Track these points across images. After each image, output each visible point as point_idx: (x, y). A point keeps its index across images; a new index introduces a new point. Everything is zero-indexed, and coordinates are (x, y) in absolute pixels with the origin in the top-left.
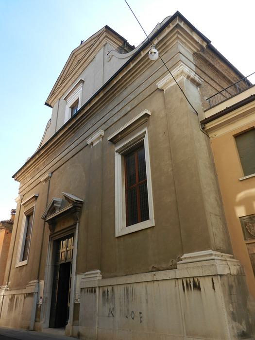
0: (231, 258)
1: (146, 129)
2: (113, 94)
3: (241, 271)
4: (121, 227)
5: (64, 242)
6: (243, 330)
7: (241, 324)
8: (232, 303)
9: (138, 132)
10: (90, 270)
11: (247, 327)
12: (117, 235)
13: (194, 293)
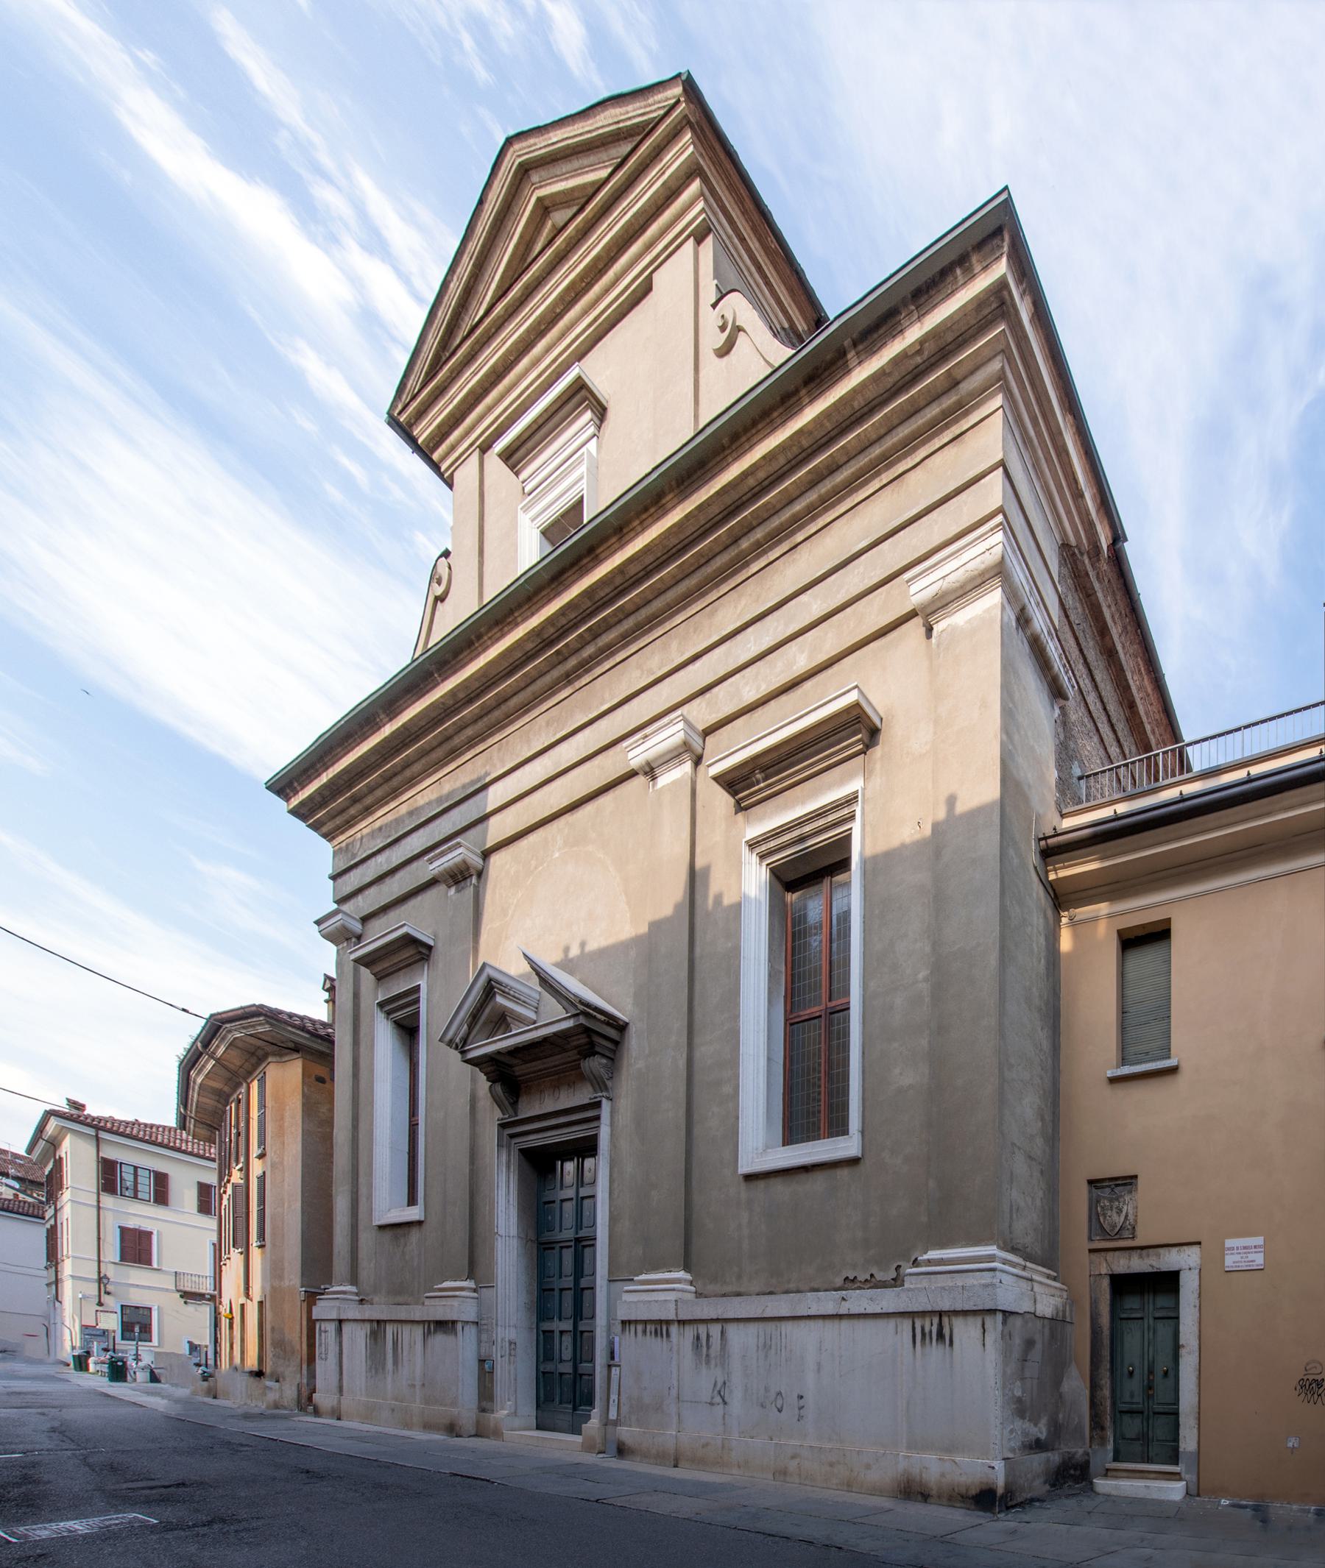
0: (1048, 1277)
2: (732, 552)
3: (1064, 1311)
4: (758, 1142)
5: (570, 1167)
7: (1036, 1425)
8: (1023, 1379)
9: (830, 787)
10: (655, 1268)
11: (1049, 1431)
12: (744, 1168)
13: (936, 1351)
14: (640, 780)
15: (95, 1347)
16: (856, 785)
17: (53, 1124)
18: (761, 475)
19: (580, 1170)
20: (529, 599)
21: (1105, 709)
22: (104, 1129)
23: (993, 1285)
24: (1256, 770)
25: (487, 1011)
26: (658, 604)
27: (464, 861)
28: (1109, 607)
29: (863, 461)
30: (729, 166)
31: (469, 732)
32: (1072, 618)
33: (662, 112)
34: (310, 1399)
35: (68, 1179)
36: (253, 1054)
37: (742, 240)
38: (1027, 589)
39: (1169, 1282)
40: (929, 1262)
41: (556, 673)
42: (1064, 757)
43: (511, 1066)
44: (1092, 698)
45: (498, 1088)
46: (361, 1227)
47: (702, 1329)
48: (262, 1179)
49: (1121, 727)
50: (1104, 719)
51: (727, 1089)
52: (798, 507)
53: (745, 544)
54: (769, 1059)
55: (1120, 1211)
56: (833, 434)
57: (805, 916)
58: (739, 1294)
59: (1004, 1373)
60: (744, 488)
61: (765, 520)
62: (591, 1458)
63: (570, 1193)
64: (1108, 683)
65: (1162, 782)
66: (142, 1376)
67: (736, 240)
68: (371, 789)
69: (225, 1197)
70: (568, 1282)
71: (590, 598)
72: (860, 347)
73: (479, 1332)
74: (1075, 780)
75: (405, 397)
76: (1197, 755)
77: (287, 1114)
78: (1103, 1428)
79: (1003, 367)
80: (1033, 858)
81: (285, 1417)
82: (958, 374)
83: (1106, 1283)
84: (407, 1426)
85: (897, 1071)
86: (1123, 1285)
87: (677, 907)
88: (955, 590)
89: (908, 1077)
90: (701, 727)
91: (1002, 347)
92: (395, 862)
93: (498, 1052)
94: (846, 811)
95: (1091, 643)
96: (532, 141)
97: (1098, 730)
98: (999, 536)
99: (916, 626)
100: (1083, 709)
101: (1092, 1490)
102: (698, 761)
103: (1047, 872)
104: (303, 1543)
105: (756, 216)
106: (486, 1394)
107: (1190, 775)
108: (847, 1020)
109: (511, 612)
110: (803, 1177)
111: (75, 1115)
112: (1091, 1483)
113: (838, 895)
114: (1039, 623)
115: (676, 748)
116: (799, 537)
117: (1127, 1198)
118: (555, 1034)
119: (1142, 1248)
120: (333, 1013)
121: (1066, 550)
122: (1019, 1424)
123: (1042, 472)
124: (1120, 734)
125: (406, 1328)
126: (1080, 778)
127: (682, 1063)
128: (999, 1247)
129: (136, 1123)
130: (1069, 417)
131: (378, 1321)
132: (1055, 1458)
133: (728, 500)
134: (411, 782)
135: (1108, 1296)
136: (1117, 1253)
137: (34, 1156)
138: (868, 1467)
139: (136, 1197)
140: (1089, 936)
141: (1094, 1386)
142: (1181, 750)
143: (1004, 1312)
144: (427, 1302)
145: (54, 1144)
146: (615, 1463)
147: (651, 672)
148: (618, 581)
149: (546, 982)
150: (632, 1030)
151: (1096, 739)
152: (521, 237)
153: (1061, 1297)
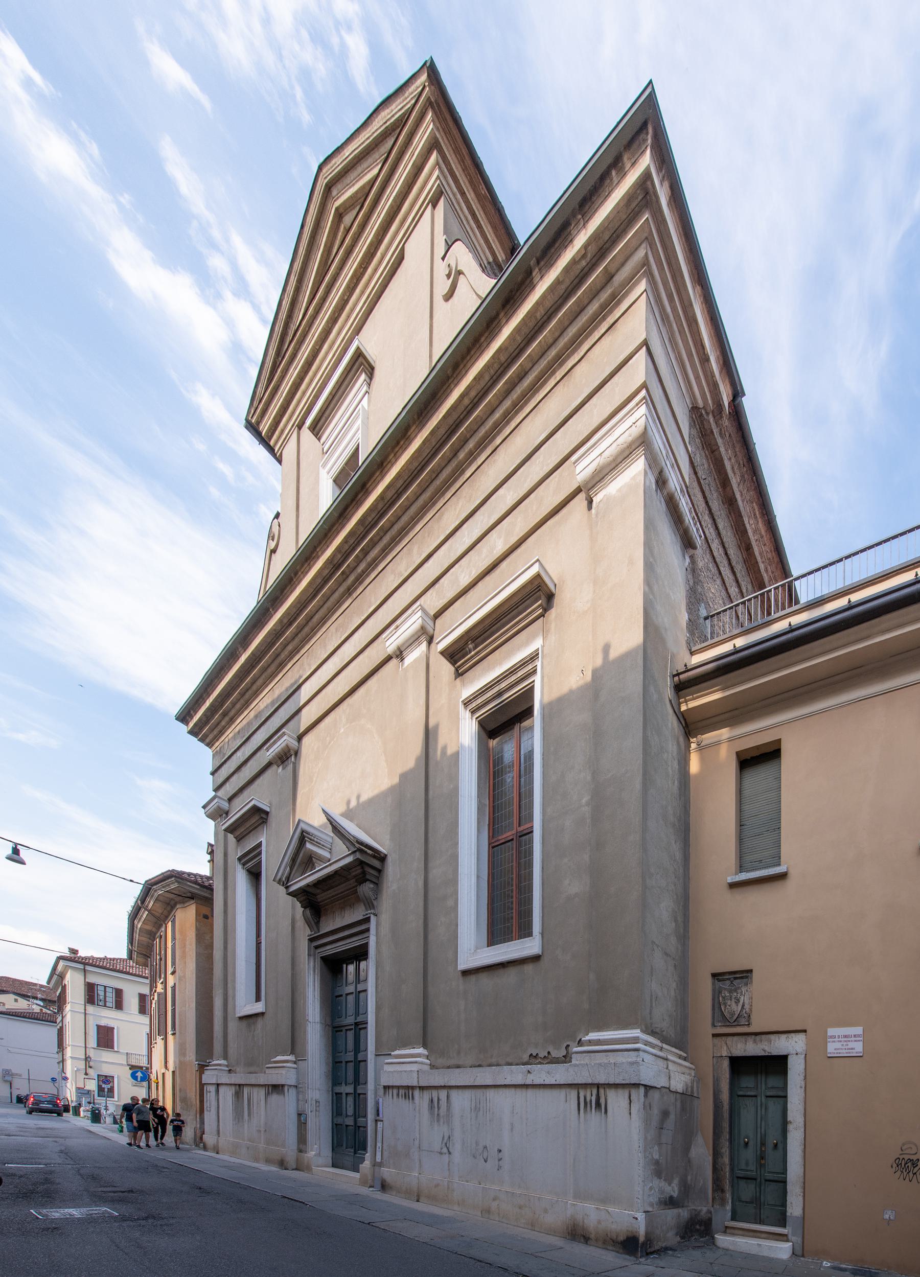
0: (680, 1057)
1: (537, 644)
3: (692, 1088)
4: (472, 948)
5: (351, 968)
6: (672, 1193)
7: (670, 1184)
9: (519, 648)
10: (405, 1045)
11: (680, 1191)
12: (462, 966)
13: (594, 1117)
14: (394, 662)
15: (84, 1101)
16: (537, 644)
17: (62, 964)
18: (473, 394)
19: (358, 970)
20: (326, 535)
21: (726, 554)
22: (88, 964)
23: (636, 1063)
24: (856, 597)
25: (301, 855)
26: (405, 519)
27: (287, 746)
28: (730, 459)
29: (543, 363)
30: (455, 131)
31: (290, 647)
32: (700, 474)
33: (413, 101)
34: (201, 1138)
35: (69, 998)
36: (168, 904)
37: (463, 194)
38: (664, 452)
39: (777, 1065)
40: (590, 1042)
41: (341, 589)
42: (693, 600)
43: (315, 895)
44: (715, 545)
45: (308, 912)
46: (229, 1019)
47: (435, 1093)
48: (174, 988)
49: (739, 568)
50: (726, 562)
51: (450, 903)
52: (497, 415)
53: (462, 455)
54: (478, 877)
55: (737, 1001)
56: (522, 345)
57: (502, 757)
58: (458, 1067)
59: (646, 1138)
60: (461, 408)
61: (475, 432)
62: (365, 1191)
63: (351, 989)
64: (729, 529)
65: (774, 616)
66: (109, 1120)
67: (459, 196)
68: (234, 704)
69: (154, 1002)
70: (350, 1056)
71: (362, 525)
72: (542, 263)
73: (298, 1093)
74: (702, 620)
75: (255, 404)
76: (804, 587)
77: (187, 943)
78: (723, 1191)
79: (646, 253)
80: (669, 692)
81: (187, 1150)
82: (612, 270)
83: (726, 1064)
84: (256, 1160)
85: (567, 882)
86: (741, 1066)
87: (418, 760)
88: (609, 464)
89: (574, 886)
90: (432, 613)
91: (646, 235)
92: (248, 754)
93: (308, 885)
94: (530, 667)
95: (715, 495)
96: (333, 162)
97: (720, 573)
98: (643, 409)
99: (580, 501)
100: (708, 556)
101: (714, 1243)
102: (430, 641)
103: (679, 704)
104: (198, 1238)
105: (472, 170)
106: (302, 1139)
107: (794, 608)
108: (531, 841)
109: (315, 548)
110: (501, 971)
111: (72, 958)
112: (713, 1238)
113: (524, 738)
114: (674, 482)
115: (416, 633)
116: (498, 440)
117: (744, 989)
118: (342, 868)
119: (756, 1034)
120: (213, 869)
121: (695, 411)
122: (657, 1183)
123: (676, 344)
124: (738, 575)
125: (256, 1090)
126: (706, 618)
127: (421, 883)
128: (642, 1031)
129: (105, 958)
130: (698, 288)
131: (239, 1085)
132: (684, 1214)
133: (451, 421)
134: (256, 694)
135: (728, 1076)
136: (735, 1038)
137: (51, 986)
138: (546, 1211)
139: (105, 1006)
140: (712, 759)
141: (716, 1154)
142: (790, 586)
143: (645, 1086)
144: (268, 1071)
145: (62, 977)
146: (379, 1195)
147: (400, 574)
148: (380, 506)
149: (336, 829)
150: (389, 860)
151: (719, 582)
152: (325, 245)
153: (690, 1074)
